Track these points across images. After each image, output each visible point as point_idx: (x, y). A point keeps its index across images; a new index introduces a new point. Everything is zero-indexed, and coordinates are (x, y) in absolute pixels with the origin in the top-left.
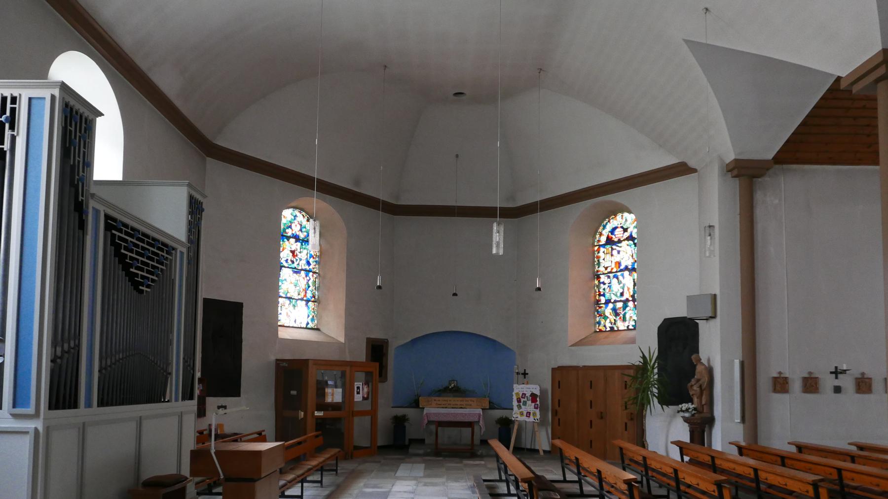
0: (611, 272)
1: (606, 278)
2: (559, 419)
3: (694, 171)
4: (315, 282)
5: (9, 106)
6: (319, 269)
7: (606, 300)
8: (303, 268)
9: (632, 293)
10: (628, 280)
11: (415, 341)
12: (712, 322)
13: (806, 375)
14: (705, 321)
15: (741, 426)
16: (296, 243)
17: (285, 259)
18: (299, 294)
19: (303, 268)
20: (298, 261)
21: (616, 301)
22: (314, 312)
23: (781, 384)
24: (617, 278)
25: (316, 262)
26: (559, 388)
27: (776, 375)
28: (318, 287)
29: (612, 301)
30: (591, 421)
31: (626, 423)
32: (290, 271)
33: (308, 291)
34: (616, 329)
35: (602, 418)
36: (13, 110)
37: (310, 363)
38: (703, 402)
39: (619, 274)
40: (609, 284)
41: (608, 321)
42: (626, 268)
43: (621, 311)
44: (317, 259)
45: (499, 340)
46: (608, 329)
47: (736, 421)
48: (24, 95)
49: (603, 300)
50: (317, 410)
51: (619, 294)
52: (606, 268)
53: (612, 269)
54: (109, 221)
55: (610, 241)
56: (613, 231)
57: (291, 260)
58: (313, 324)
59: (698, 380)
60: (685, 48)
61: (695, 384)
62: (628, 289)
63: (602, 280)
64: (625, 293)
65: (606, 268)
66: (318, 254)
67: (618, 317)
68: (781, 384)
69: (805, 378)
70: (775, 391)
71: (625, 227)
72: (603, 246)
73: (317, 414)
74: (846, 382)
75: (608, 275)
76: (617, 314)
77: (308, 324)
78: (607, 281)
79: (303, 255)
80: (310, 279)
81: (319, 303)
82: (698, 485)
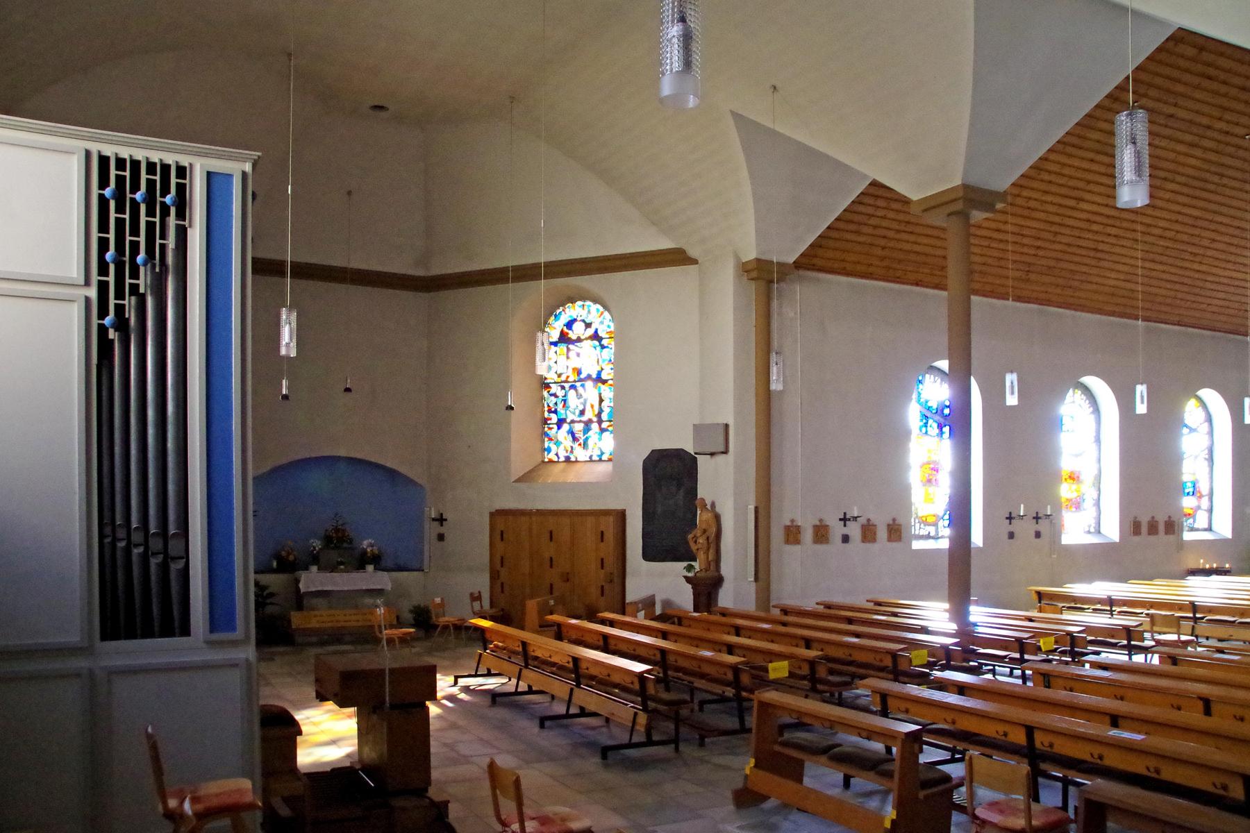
0: (566, 381)
1: (559, 388)
2: (502, 584)
3: (694, 262)
5: (174, 181)
7: (558, 419)
9: (596, 412)
10: (590, 392)
12: (720, 459)
13: (818, 523)
15: (754, 584)
21: (573, 422)
23: (792, 534)
24: (576, 390)
26: (502, 540)
27: (788, 523)
29: (568, 420)
30: (551, 585)
31: (602, 587)
34: (573, 459)
36: (181, 189)
39: (578, 384)
40: (563, 397)
41: (562, 447)
42: (589, 377)
43: (582, 436)
45: (403, 469)
46: (562, 459)
47: (750, 579)
48: (199, 168)
51: (577, 412)
52: (559, 376)
53: (568, 377)
54: (1022, 506)
55: (564, 338)
56: (570, 325)
59: (705, 531)
60: (731, 122)
62: (592, 406)
63: (552, 391)
64: (586, 412)
65: (559, 376)
67: (577, 444)
68: (792, 534)
69: (817, 526)
70: (787, 542)
71: (588, 321)
72: (555, 344)
74: (854, 530)
75: (562, 384)
76: (575, 439)
82: (550, 657)
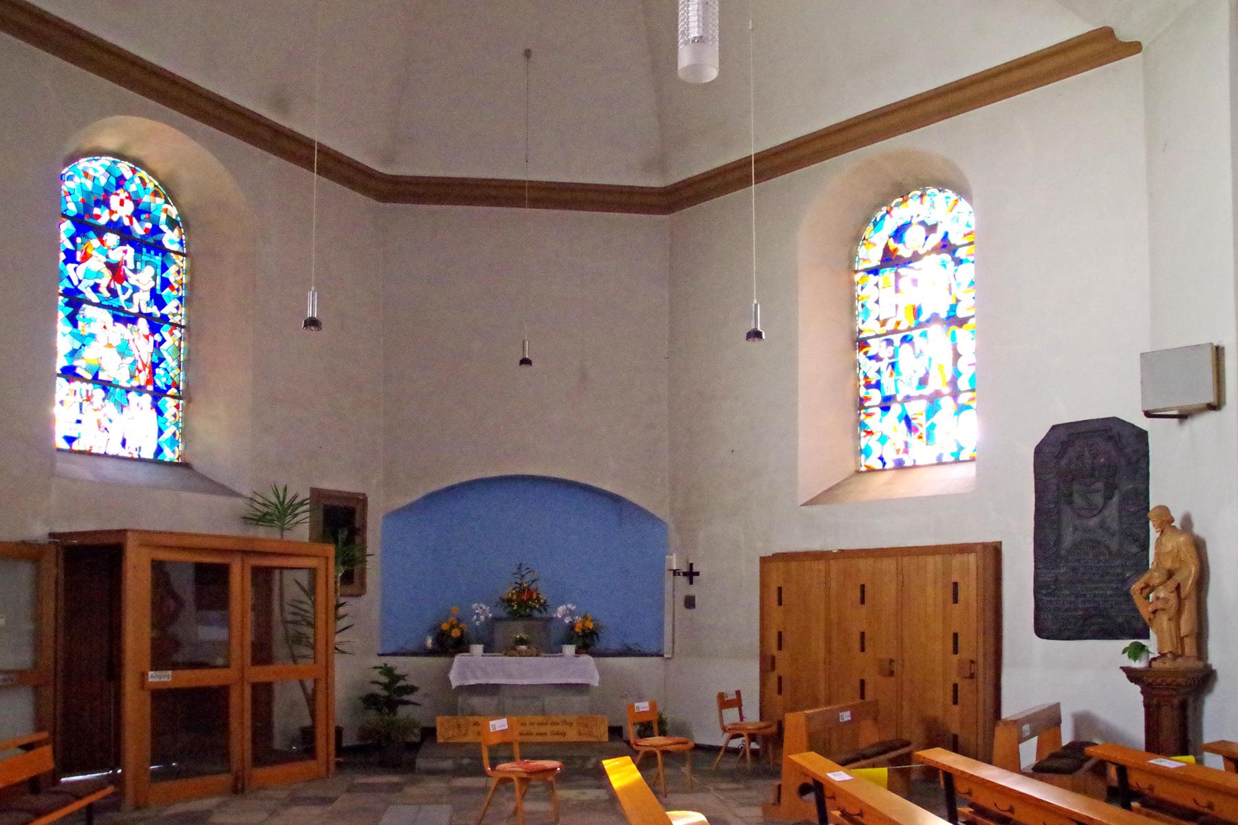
0: (895, 331)
3: (1135, 48)
4: (179, 348)
6: (188, 316)
8: (145, 310)
11: (433, 498)
14: (1175, 420)
16: (123, 248)
17: (92, 283)
18: (132, 377)
19: (144, 311)
20: (130, 291)
21: (908, 398)
22: (176, 424)
25: (180, 299)
26: (780, 603)
28: (184, 361)
29: (899, 398)
30: (862, 683)
31: (955, 686)
32: (106, 316)
33: (157, 370)
35: (892, 673)
37: (131, 544)
38: (1183, 631)
39: (915, 334)
40: (890, 358)
42: (934, 318)
44: (182, 293)
49: (875, 397)
50: (156, 667)
52: (884, 323)
55: (890, 259)
56: (898, 234)
57: (109, 288)
58: (174, 452)
61: (1161, 584)
62: (941, 368)
65: (884, 323)
66: (184, 281)
71: (930, 223)
73: (154, 677)
75: (888, 337)
77: (159, 450)
78: (885, 352)
79: (145, 279)
80: (164, 341)
81: (189, 401)
